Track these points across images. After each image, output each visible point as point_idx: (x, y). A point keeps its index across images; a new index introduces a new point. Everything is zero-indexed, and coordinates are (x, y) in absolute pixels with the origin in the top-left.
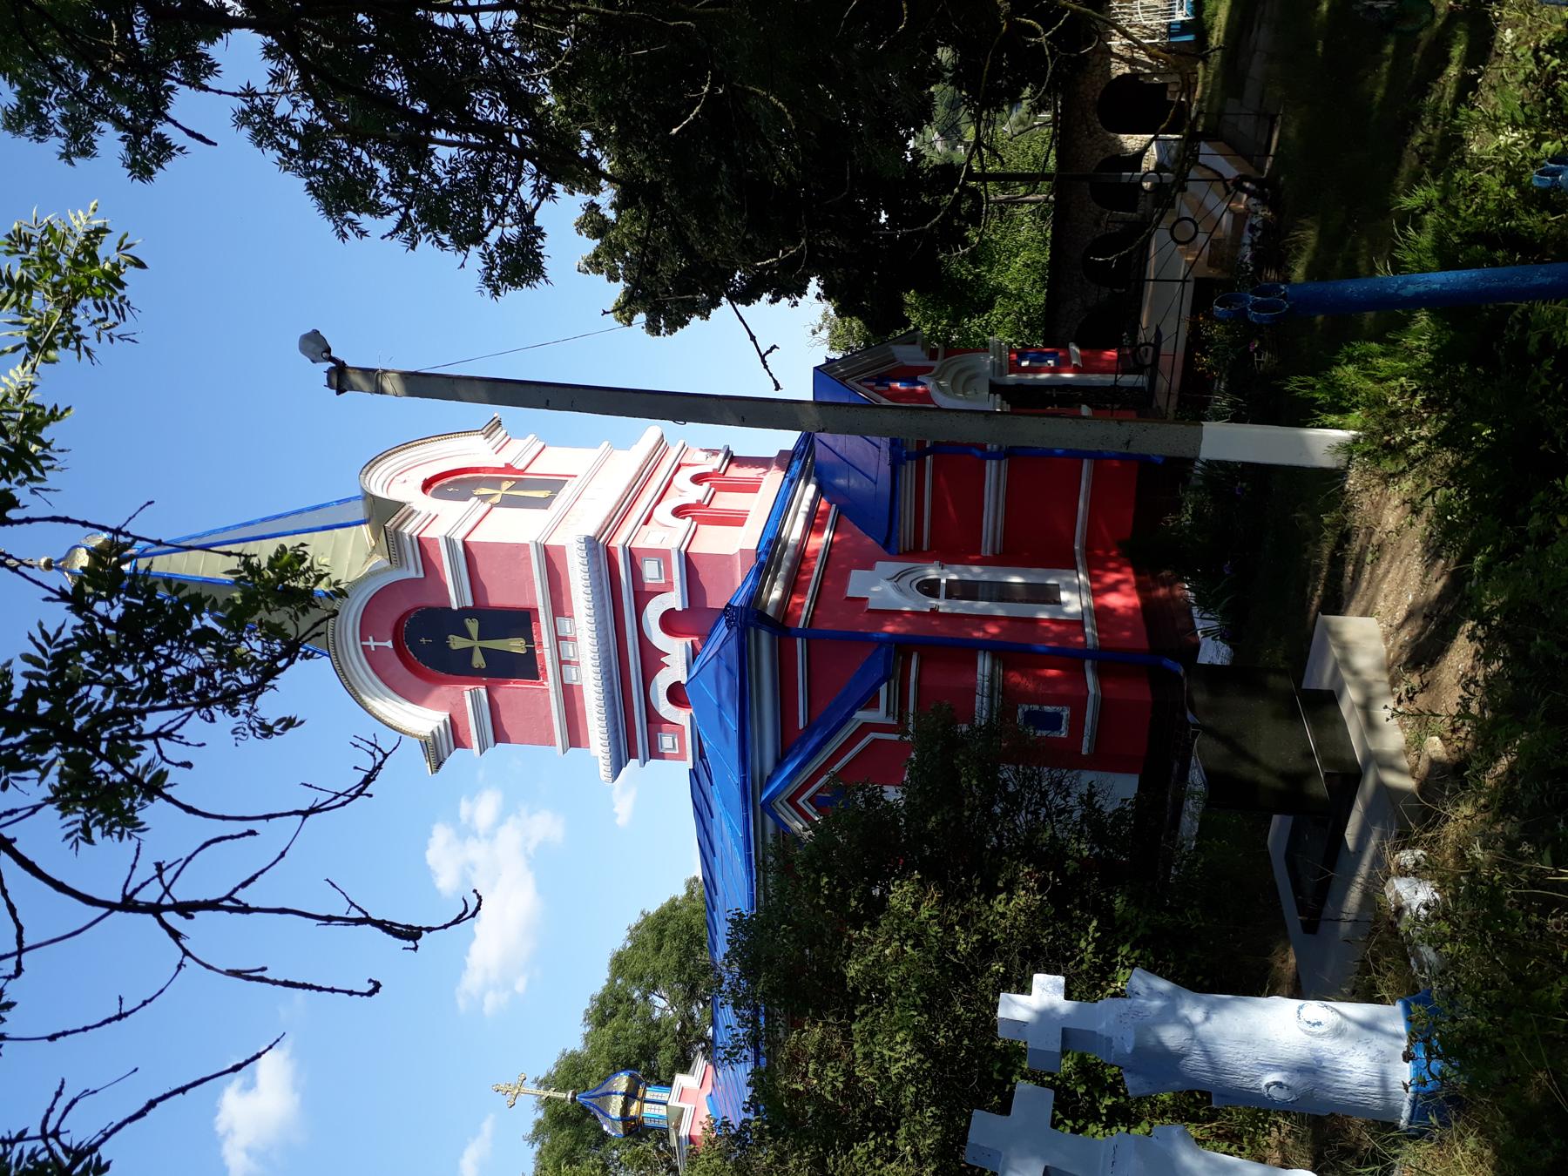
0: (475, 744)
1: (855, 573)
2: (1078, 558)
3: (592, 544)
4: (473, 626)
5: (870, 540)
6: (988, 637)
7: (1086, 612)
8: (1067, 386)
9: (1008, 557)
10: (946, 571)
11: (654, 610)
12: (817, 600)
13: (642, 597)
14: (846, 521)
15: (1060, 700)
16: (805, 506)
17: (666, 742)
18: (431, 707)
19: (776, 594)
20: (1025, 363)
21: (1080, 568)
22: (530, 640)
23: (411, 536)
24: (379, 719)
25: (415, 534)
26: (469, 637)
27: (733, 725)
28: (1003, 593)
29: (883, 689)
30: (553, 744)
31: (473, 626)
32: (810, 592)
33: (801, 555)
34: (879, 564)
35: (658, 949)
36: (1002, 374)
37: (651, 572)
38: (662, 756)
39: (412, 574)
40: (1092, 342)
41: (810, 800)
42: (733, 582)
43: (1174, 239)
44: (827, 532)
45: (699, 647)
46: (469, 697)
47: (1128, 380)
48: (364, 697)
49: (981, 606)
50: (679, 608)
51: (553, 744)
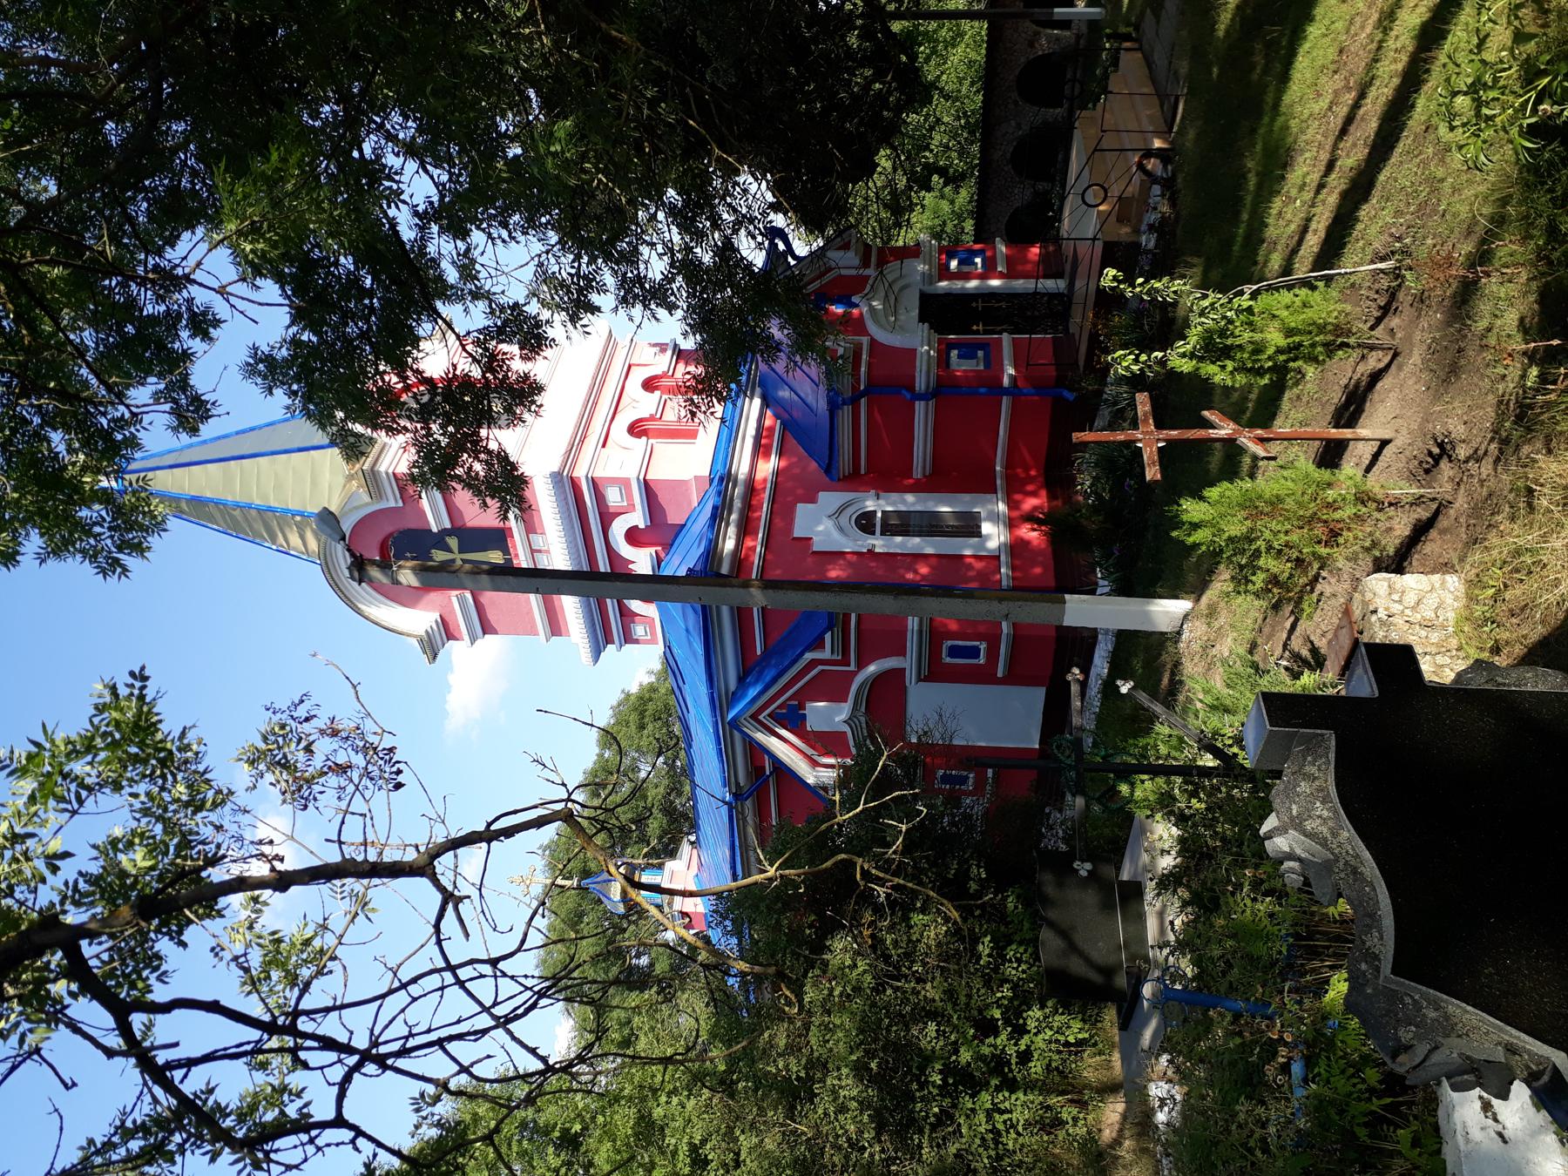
0: (466, 637)
1: (800, 506)
2: (999, 482)
3: (557, 478)
4: (453, 542)
5: (814, 465)
6: (918, 578)
7: (1003, 549)
8: (993, 295)
9: (934, 483)
10: (881, 502)
11: (619, 528)
12: (767, 543)
13: (607, 518)
14: (792, 442)
15: (979, 638)
16: (751, 430)
17: (639, 630)
18: (425, 609)
19: (730, 545)
20: (954, 264)
21: (999, 496)
22: (506, 551)
23: (387, 473)
24: (376, 624)
25: (390, 471)
26: (450, 551)
27: (700, 650)
28: (930, 525)
29: (828, 636)
30: (536, 634)
31: (453, 542)
32: (760, 535)
33: (751, 488)
34: (822, 495)
35: (642, 727)
36: (931, 283)
37: (613, 497)
38: (637, 642)
39: (392, 504)
40: (1018, 237)
41: (769, 715)
42: (690, 503)
43: (1084, 202)
44: (773, 456)
45: (662, 555)
46: (456, 601)
47: (1049, 285)
48: (360, 606)
49: (914, 544)
50: (642, 526)
51: (536, 634)
